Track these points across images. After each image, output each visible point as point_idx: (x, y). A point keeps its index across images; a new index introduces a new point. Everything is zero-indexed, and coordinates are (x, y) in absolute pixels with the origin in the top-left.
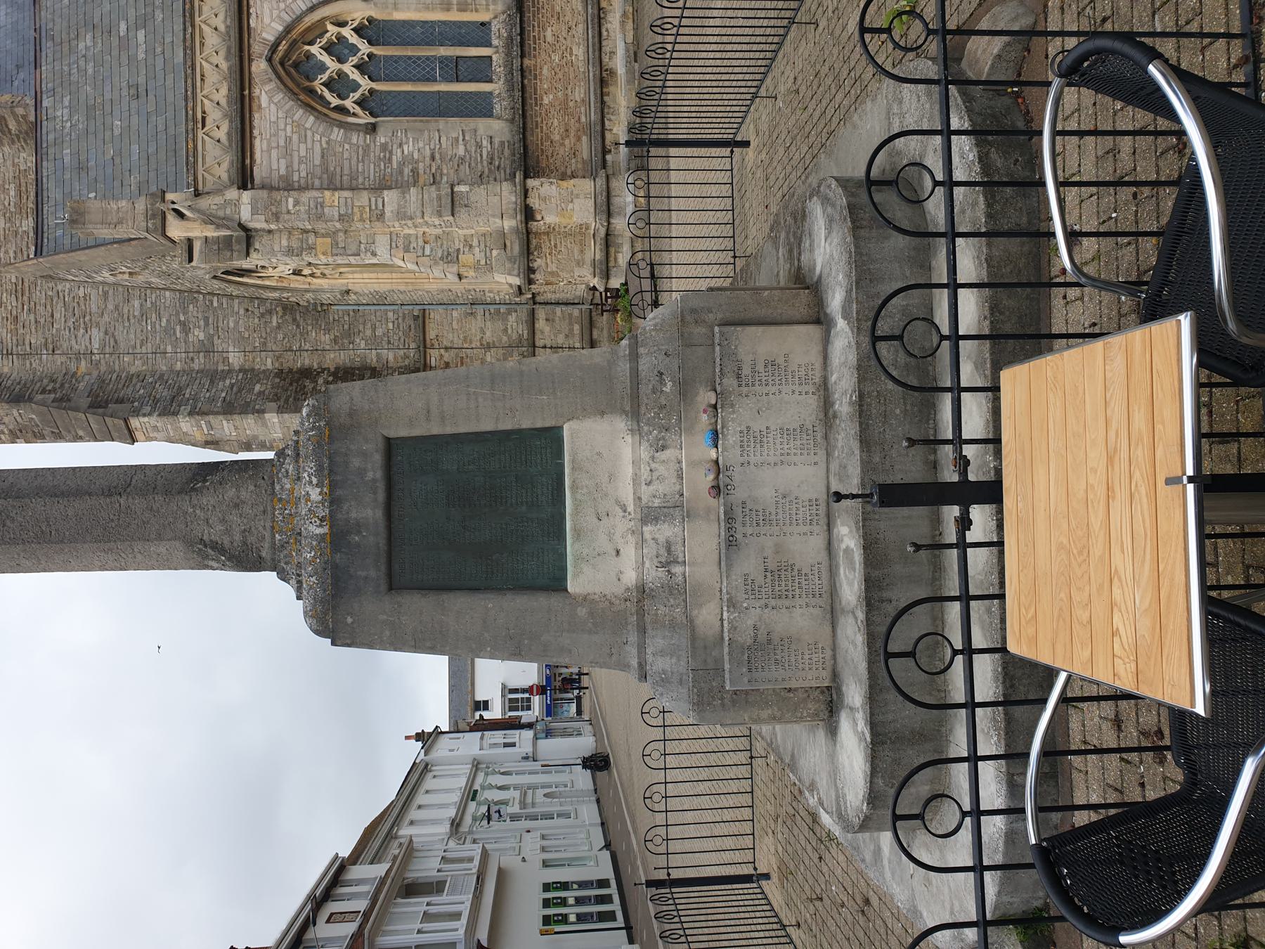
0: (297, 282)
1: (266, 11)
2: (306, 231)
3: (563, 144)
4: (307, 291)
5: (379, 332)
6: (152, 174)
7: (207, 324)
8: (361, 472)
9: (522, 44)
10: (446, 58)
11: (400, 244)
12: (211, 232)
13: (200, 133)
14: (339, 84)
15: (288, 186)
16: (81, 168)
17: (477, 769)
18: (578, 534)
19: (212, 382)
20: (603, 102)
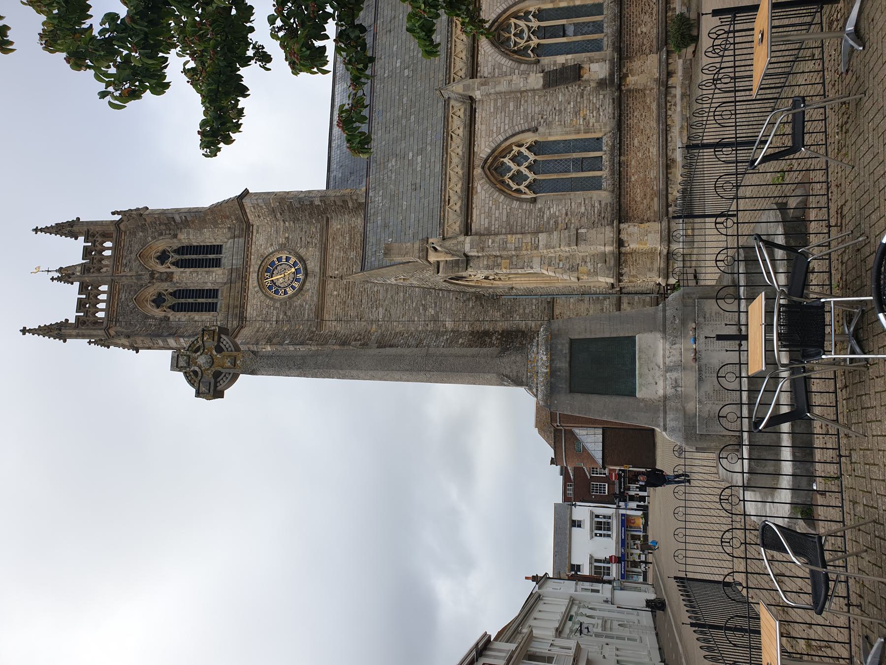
0: (486, 284)
1: (483, 143)
2: (496, 256)
3: (642, 203)
4: (490, 288)
5: (527, 311)
6: (420, 229)
7: (436, 306)
8: (561, 350)
9: (620, 149)
10: (576, 159)
11: (546, 262)
12: (449, 258)
13: (447, 207)
14: (518, 177)
15: (489, 233)
16: (386, 226)
17: (573, 603)
18: (640, 376)
19: (437, 337)
20: (667, 178)
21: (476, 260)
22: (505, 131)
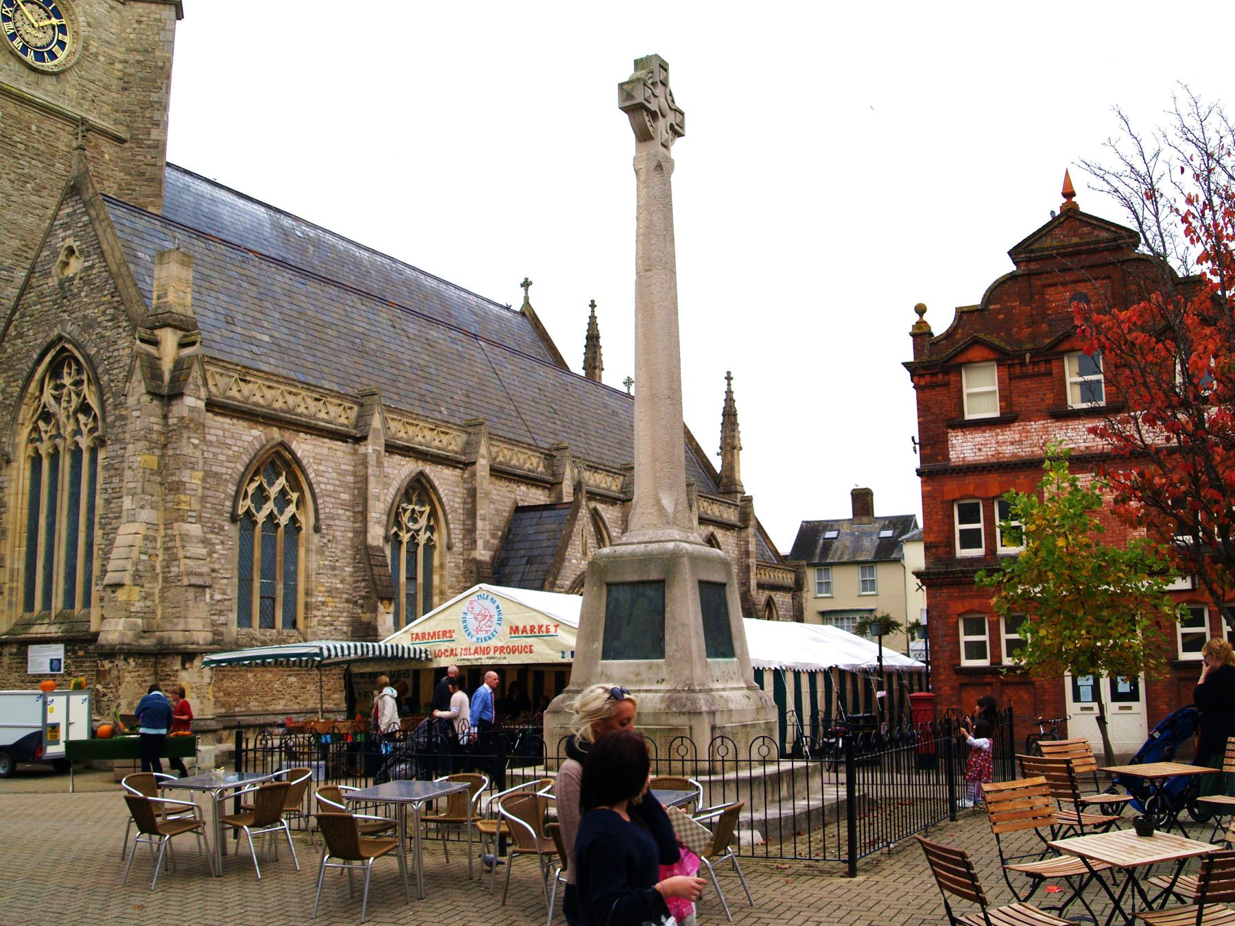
14: (261, 496)
21: (158, 411)
22: (320, 482)
